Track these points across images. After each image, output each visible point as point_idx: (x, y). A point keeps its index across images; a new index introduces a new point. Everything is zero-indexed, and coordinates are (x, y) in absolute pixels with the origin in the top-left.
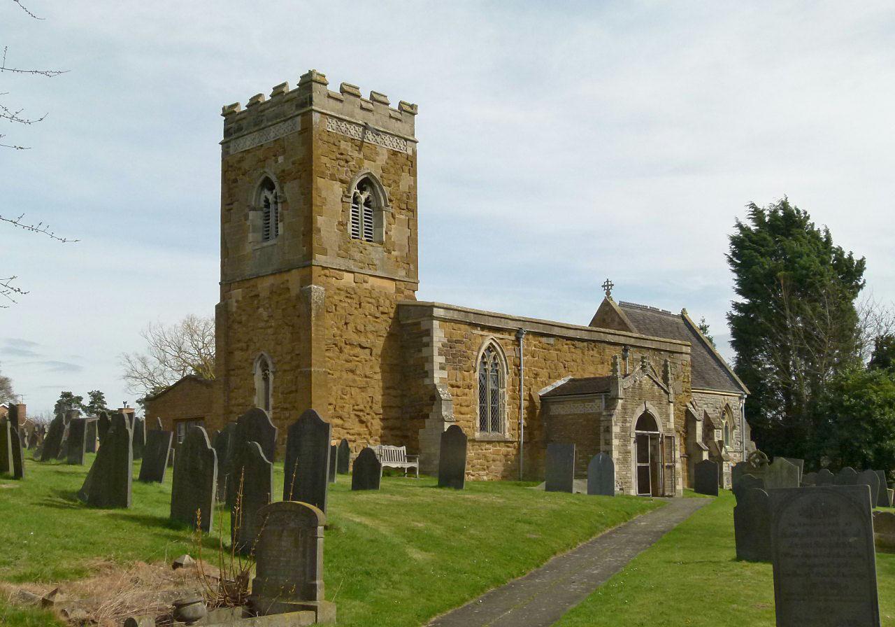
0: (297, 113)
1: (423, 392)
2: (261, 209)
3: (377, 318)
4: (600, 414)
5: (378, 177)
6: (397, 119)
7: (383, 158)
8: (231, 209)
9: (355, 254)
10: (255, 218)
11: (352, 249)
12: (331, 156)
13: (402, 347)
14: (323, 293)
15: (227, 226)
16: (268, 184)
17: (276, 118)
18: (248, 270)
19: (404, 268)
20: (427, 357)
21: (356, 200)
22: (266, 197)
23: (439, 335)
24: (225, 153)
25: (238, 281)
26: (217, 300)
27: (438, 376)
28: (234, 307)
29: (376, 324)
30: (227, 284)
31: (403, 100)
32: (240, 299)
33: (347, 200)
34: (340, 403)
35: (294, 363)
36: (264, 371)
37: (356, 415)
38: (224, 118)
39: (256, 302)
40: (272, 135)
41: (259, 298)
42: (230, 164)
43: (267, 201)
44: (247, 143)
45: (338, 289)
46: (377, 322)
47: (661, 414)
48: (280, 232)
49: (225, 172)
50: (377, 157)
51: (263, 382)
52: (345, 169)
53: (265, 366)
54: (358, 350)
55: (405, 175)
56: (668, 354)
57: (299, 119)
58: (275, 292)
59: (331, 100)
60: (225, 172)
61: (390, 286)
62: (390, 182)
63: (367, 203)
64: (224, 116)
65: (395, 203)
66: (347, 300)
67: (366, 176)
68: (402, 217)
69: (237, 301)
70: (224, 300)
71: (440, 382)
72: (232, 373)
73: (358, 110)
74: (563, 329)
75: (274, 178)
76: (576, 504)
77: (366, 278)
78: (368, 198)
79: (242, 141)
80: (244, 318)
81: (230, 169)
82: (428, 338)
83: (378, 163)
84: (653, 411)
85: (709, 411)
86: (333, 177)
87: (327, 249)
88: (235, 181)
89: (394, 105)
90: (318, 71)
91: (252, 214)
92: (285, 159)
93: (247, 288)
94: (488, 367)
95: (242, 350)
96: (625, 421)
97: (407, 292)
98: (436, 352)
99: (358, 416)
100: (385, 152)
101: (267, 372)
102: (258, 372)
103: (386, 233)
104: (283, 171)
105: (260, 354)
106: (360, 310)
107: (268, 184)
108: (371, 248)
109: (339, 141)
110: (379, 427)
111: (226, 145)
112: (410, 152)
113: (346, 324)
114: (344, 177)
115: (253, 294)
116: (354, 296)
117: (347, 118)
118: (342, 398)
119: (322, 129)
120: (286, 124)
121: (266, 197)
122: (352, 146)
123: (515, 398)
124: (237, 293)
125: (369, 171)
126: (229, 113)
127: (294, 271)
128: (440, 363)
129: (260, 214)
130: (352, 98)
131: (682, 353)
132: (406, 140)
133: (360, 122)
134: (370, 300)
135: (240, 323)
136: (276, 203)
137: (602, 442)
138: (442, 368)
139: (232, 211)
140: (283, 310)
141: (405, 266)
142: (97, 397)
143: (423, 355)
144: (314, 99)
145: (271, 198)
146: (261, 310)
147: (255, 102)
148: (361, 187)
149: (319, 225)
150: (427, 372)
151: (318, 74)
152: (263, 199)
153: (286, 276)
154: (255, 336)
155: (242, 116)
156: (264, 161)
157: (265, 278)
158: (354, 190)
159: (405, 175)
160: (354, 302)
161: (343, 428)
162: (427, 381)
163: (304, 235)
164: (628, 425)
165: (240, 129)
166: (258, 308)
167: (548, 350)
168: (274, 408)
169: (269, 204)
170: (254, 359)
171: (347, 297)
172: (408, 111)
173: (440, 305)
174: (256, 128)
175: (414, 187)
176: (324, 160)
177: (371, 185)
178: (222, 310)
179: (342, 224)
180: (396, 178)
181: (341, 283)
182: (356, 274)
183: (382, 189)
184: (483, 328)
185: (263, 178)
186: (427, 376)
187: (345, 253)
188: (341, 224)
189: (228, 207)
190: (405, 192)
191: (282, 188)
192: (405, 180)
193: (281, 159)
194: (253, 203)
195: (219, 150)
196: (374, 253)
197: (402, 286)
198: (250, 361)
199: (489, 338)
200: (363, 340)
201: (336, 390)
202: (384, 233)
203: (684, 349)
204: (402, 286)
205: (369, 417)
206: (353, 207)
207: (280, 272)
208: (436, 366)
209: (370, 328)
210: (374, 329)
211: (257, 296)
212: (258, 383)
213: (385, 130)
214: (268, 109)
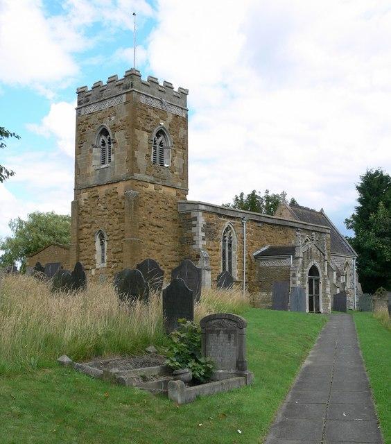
2: (165, 148)
4: (290, 266)
5: (167, 129)
7: (170, 119)
10: (97, 152)
13: (180, 227)
23: (202, 221)
24: (79, 115)
26: (73, 199)
27: (201, 244)
28: (82, 202)
30: (78, 190)
31: (181, 87)
40: (107, 105)
43: (103, 142)
48: (112, 160)
53: (102, 237)
54: (156, 229)
55: (182, 129)
61: (173, 192)
63: (161, 144)
72: (81, 241)
73: (156, 91)
75: (109, 130)
80: (89, 210)
84: (318, 265)
85: (338, 265)
86: (144, 129)
89: (176, 89)
92: (116, 118)
94: (227, 238)
95: (88, 228)
96: (303, 271)
97: (182, 196)
102: (98, 241)
104: (115, 125)
106: (158, 206)
107: (104, 132)
110: (239, 293)
112: (184, 116)
113: (150, 213)
115: (95, 195)
123: (241, 256)
124: (85, 195)
126: (81, 92)
132: (182, 109)
136: (109, 143)
137: (291, 282)
138: (203, 239)
140: (114, 204)
147: (97, 86)
148: (158, 135)
153: (115, 186)
155: (89, 93)
158: (154, 136)
159: (182, 129)
160: (154, 201)
162: (194, 247)
165: (88, 101)
172: (183, 93)
175: (186, 136)
177: (164, 134)
178: (75, 205)
179: (148, 156)
184: (225, 216)
188: (148, 156)
193: (113, 118)
195: (75, 113)
199: (227, 223)
200: (158, 223)
203: (327, 231)
204: (179, 192)
212: (98, 246)
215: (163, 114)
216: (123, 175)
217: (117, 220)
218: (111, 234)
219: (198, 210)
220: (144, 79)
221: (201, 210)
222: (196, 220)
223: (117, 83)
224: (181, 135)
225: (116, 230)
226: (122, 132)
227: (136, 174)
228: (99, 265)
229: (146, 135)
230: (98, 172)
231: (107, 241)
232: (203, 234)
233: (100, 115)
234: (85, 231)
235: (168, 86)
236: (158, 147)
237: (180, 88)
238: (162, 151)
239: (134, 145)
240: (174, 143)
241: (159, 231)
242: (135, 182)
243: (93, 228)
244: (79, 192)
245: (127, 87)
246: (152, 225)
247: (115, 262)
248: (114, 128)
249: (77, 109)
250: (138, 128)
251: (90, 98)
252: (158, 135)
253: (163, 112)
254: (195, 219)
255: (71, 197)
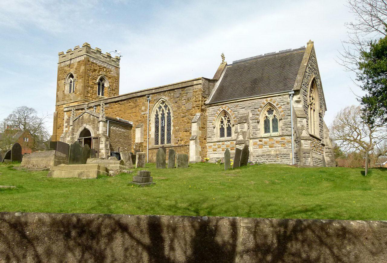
47: (93, 128)
56: (181, 90)
74: (112, 99)
76: (151, 164)
98: (65, 122)
131: (193, 86)
145: (72, 80)
152: (70, 80)
164: (74, 136)
167: (107, 109)
172: (61, 54)
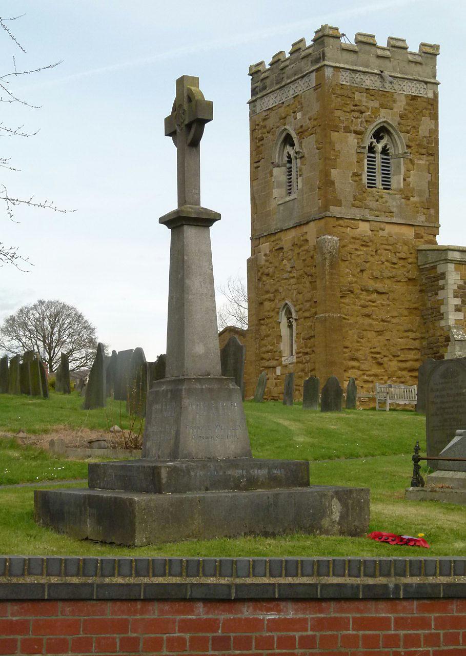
0: (311, 69)
1: (439, 334)
3: (394, 264)
6: (416, 63)
7: (400, 105)
8: (259, 167)
9: (371, 203)
10: (279, 174)
11: (369, 198)
12: (345, 109)
13: (421, 291)
14: (336, 243)
15: (255, 183)
16: (288, 140)
17: (295, 75)
18: (274, 226)
19: (424, 213)
20: (443, 300)
21: (371, 149)
22: (288, 153)
24: (253, 113)
25: (265, 236)
26: (248, 254)
29: (393, 270)
30: (256, 239)
32: (268, 252)
33: (362, 151)
34: (356, 345)
35: (313, 310)
36: (288, 319)
37: (372, 357)
38: (251, 77)
39: (281, 254)
40: (291, 92)
41: (284, 251)
42: (257, 123)
43: (289, 156)
44: (271, 101)
45: (354, 238)
46: (394, 268)
49: (253, 131)
50: (394, 105)
51: (288, 329)
52: (360, 120)
53: (289, 314)
54: (375, 296)
57: (314, 75)
58: (297, 244)
59: (345, 53)
60: (253, 131)
61: (409, 233)
62: (409, 128)
63: (385, 151)
64: (250, 75)
65: (415, 149)
66: (362, 248)
67: (382, 125)
68: (422, 162)
69: (265, 255)
70: (254, 254)
71: (456, 324)
73: (373, 59)
75: (294, 135)
77: (382, 226)
78: (386, 146)
79: (267, 100)
81: (257, 127)
82: (444, 280)
83: (395, 110)
86: (347, 130)
87: (341, 200)
88: (262, 139)
90: (330, 25)
91: (276, 171)
92: (303, 115)
93: (273, 242)
95: (271, 300)
97: (426, 237)
99: (375, 358)
100: (403, 98)
101: (291, 319)
103: (404, 180)
105: (284, 303)
106: (377, 257)
107: (288, 140)
108: (388, 196)
109: (353, 93)
111: (252, 104)
112: (431, 95)
114: (359, 128)
116: (370, 244)
117: (362, 69)
118: (358, 342)
119: (334, 83)
120: (304, 80)
121: (288, 153)
122: (367, 97)
124: (265, 247)
125: (385, 120)
126: (255, 72)
127: (312, 224)
128: (456, 305)
129: (284, 169)
130: (367, 47)
132: (426, 83)
133: (376, 71)
134: (387, 247)
135: (268, 275)
138: (458, 309)
139: (259, 168)
141: (425, 211)
142: (97, 337)
143: (440, 298)
144: (326, 54)
145: (292, 153)
146: (285, 262)
147: (277, 60)
148: (378, 136)
149: (333, 178)
150: (442, 314)
151: (331, 28)
152: (286, 155)
153: (305, 229)
154: (280, 286)
156: (285, 118)
157: (302, 227)
161: (358, 370)
163: (319, 188)
165: (264, 88)
166: (283, 260)
168: (297, 353)
169: (291, 159)
170: (279, 308)
171: (362, 245)
173: (456, 249)
174: (278, 86)
175: (435, 132)
176: (338, 113)
177: (389, 133)
178: (252, 264)
180: (414, 123)
181: (357, 232)
182: (372, 223)
183: (399, 137)
185: (284, 134)
186: (442, 319)
187: (359, 201)
188: (355, 175)
189: (256, 165)
190: (425, 137)
191: (301, 143)
192: (425, 125)
193: (299, 116)
194: (277, 160)
196: (390, 201)
197: (421, 231)
198: (276, 310)
200: (379, 286)
201: (352, 334)
202: (402, 180)
204: (421, 231)
205: (386, 359)
206: (368, 157)
207: (300, 225)
208: (451, 308)
209: (387, 273)
210: (391, 275)
211: (282, 248)
212: (284, 330)
213: (402, 76)
214: (287, 66)
215: (385, 98)
216: (313, 210)
217: (308, 285)
218: (300, 309)
219: (447, 261)
220: (349, 40)
221: (452, 261)
222: (444, 278)
223: (303, 54)
224: (423, 130)
225: (307, 301)
226: (312, 138)
227: (332, 208)
228: (286, 359)
229: (352, 139)
230: (281, 208)
231: (295, 319)
232: (458, 301)
233: (282, 111)
234: (267, 305)
235: (397, 46)
236: (379, 157)
237: (423, 45)
238: (386, 164)
239: (328, 159)
240: (409, 147)
241: (380, 300)
242: (332, 222)
243: (277, 301)
244: (257, 242)
245: (317, 61)
246: (367, 291)
247: (307, 353)
248: (302, 133)
249: (249, 103)
250: (336, 129)
251: (268, 82)
252: (378, 136)
253: (385, 94)
254: (443, 276)
255: (246, 252)
